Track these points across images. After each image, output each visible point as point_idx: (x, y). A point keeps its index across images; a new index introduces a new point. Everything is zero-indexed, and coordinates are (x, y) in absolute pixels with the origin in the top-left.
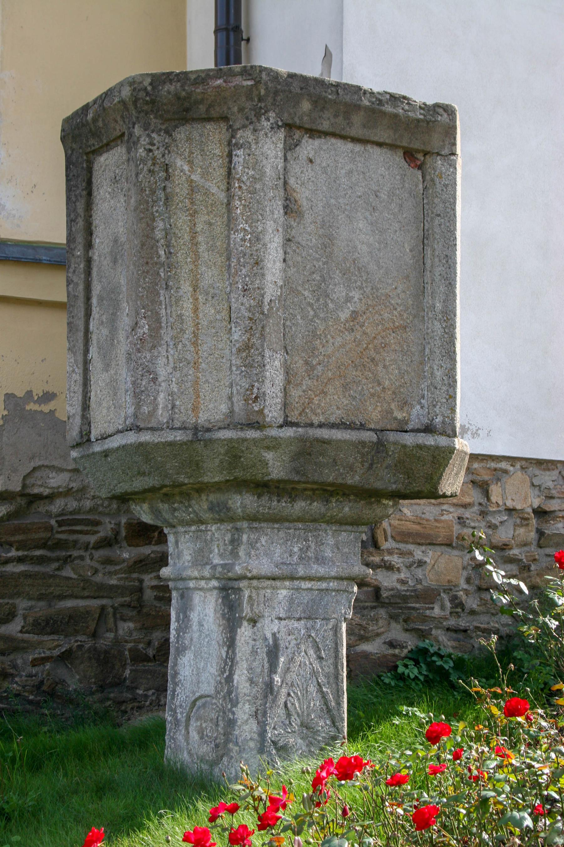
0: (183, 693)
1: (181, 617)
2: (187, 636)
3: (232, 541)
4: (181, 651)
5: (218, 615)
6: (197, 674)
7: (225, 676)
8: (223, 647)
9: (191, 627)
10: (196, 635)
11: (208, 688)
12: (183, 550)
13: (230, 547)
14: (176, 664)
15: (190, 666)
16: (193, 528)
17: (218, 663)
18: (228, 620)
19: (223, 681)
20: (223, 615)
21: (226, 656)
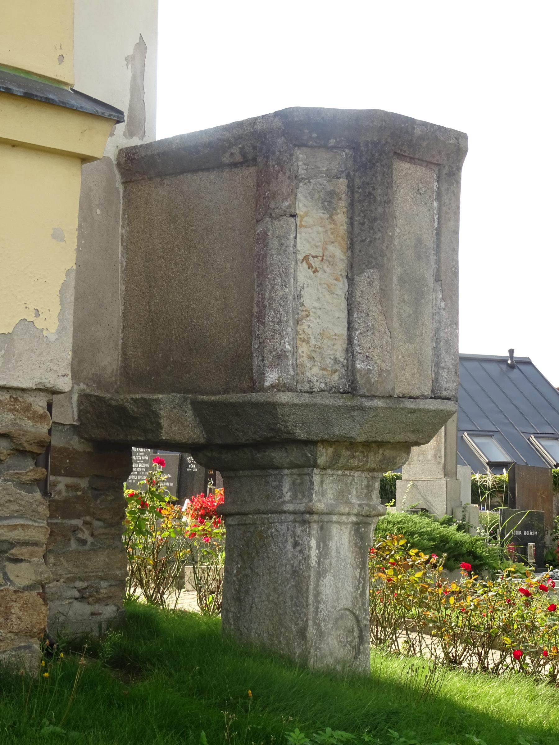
0: (325, 609)
1: (322, 545)
2: (327, 561)
3: (368, 486)
4: (321, 574)
5: (352, 544)
6: (337, 592)
7: (359, 592)
8: (356, 569)
9: (330, 553)
10: (334, 561)
11: (347, 603)
12: (326, 489)
13: (365, 491)
14: (317, 585)
15: (331, 586)
16: (340, 472)
17: (353, 582)
18: (360, 548)
19: (358, 596)
20: (356, 544)
21: (360, 577)
